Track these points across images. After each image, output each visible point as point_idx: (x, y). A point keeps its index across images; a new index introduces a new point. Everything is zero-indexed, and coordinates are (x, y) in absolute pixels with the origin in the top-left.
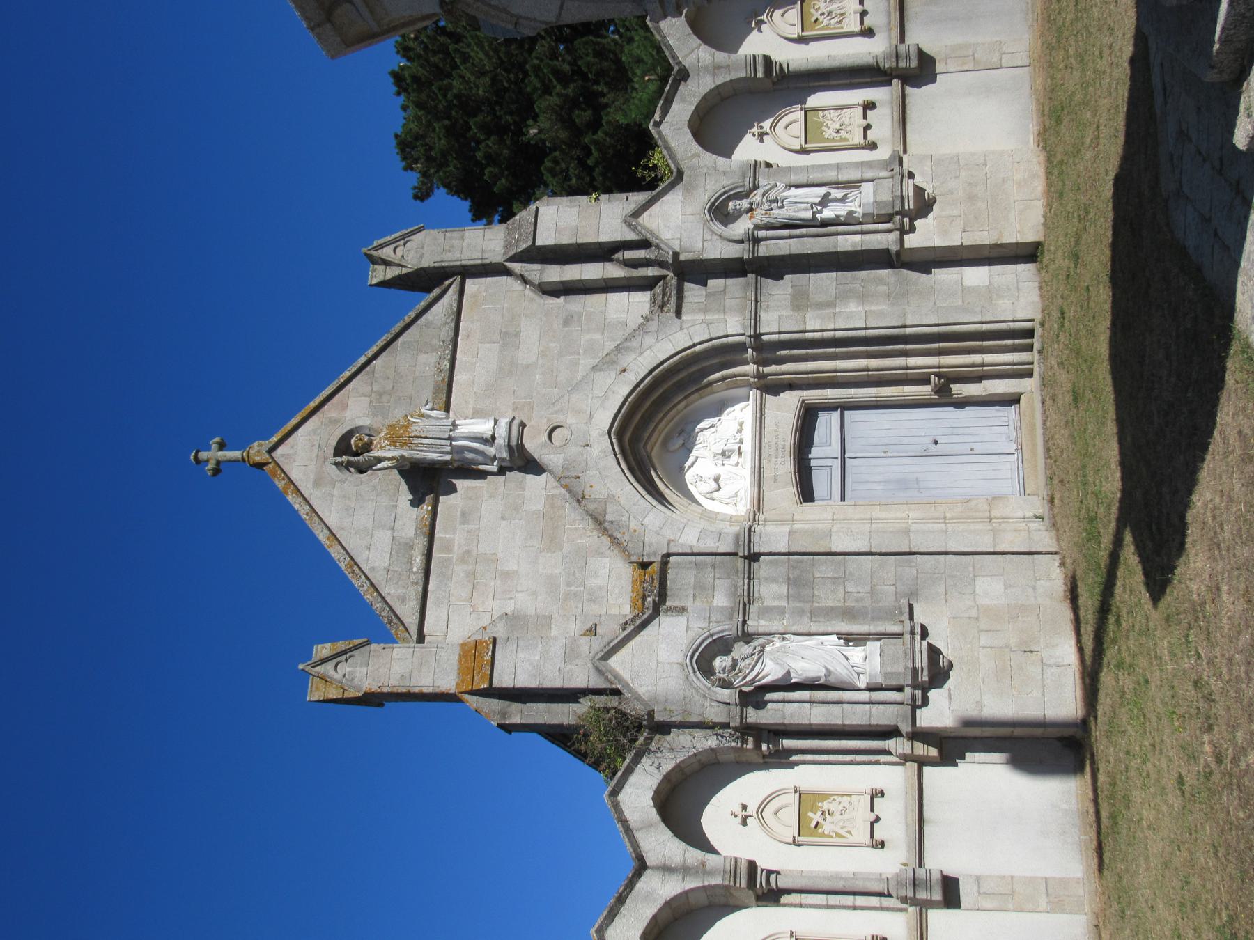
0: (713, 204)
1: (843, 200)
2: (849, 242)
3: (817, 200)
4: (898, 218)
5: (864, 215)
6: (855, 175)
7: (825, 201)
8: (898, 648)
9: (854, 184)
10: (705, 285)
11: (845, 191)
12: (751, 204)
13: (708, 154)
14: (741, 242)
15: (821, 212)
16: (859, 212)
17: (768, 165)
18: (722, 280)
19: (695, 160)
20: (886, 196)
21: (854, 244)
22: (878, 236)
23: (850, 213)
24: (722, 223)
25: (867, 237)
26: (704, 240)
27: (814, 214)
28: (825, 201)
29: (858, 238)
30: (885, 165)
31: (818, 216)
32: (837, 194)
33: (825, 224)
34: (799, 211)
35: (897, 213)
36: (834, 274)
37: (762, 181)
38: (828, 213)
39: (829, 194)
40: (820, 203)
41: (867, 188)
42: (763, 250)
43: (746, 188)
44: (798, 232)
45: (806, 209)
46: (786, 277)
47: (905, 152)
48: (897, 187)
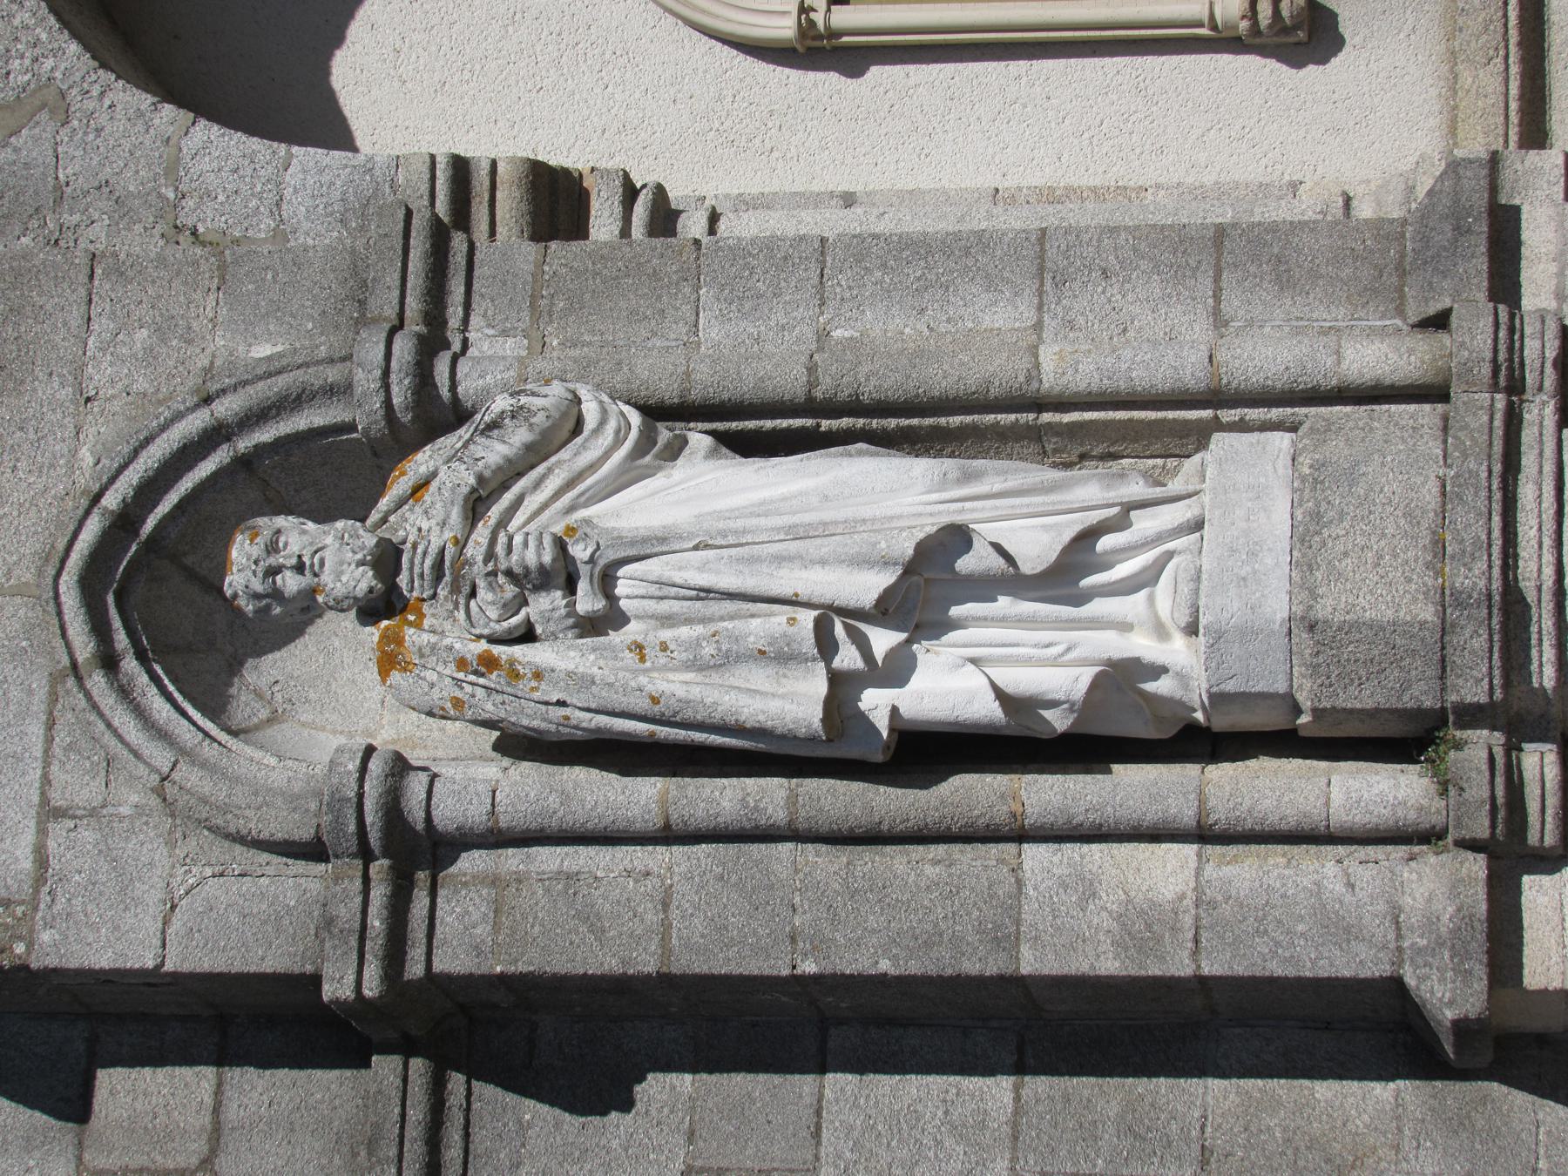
0: (125, 522)
1: (1066, 576)
2: (1107, 894)
3: (867, 587)
4: (1480, 744)
5: (1218, 699)
6: (1151, 339)
7: (930, 586)
8: (1403, 460)
9: (1158, 425)
10: (75, 1106)
11: (1091, 491)
12: (387, 559)
13: (130, 98)
14: (314, 851)
15: (896, 671)
16: (1184, 672)
17: (556, 201)
18: (197, 1081)
19: (32, 143)
20: (1386, 587)
21: (1142, 925)
22: (1323, 869)
23: (1120, 678)
24: (577, 238)
25: (1242, 871)
26: (49, 813)
27: (842, 689)
28: (930, 586)
29: (1168, 871)
30: (1378, 258)
31: (876, 703)
32: (1021, 512)
33: (927, 751)
34: (727, 660)
35: (1471, 716)
36: (997, 1091)
37: (488, 361)
38: (947, 683)
39: (957, 537)
40: (885, 610)
41: (1248, 483)
42: (465, 930)
43: (365, 413)
44: (724, 797)
45: (779, 656)
46: (657, 1089)
47: (1535, 133)
48: (1474, 523)
